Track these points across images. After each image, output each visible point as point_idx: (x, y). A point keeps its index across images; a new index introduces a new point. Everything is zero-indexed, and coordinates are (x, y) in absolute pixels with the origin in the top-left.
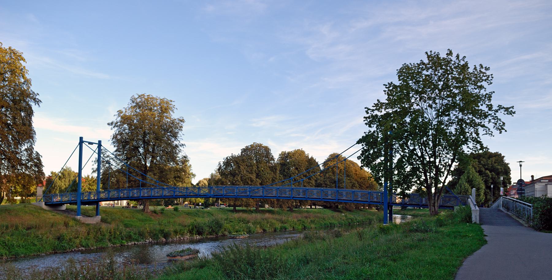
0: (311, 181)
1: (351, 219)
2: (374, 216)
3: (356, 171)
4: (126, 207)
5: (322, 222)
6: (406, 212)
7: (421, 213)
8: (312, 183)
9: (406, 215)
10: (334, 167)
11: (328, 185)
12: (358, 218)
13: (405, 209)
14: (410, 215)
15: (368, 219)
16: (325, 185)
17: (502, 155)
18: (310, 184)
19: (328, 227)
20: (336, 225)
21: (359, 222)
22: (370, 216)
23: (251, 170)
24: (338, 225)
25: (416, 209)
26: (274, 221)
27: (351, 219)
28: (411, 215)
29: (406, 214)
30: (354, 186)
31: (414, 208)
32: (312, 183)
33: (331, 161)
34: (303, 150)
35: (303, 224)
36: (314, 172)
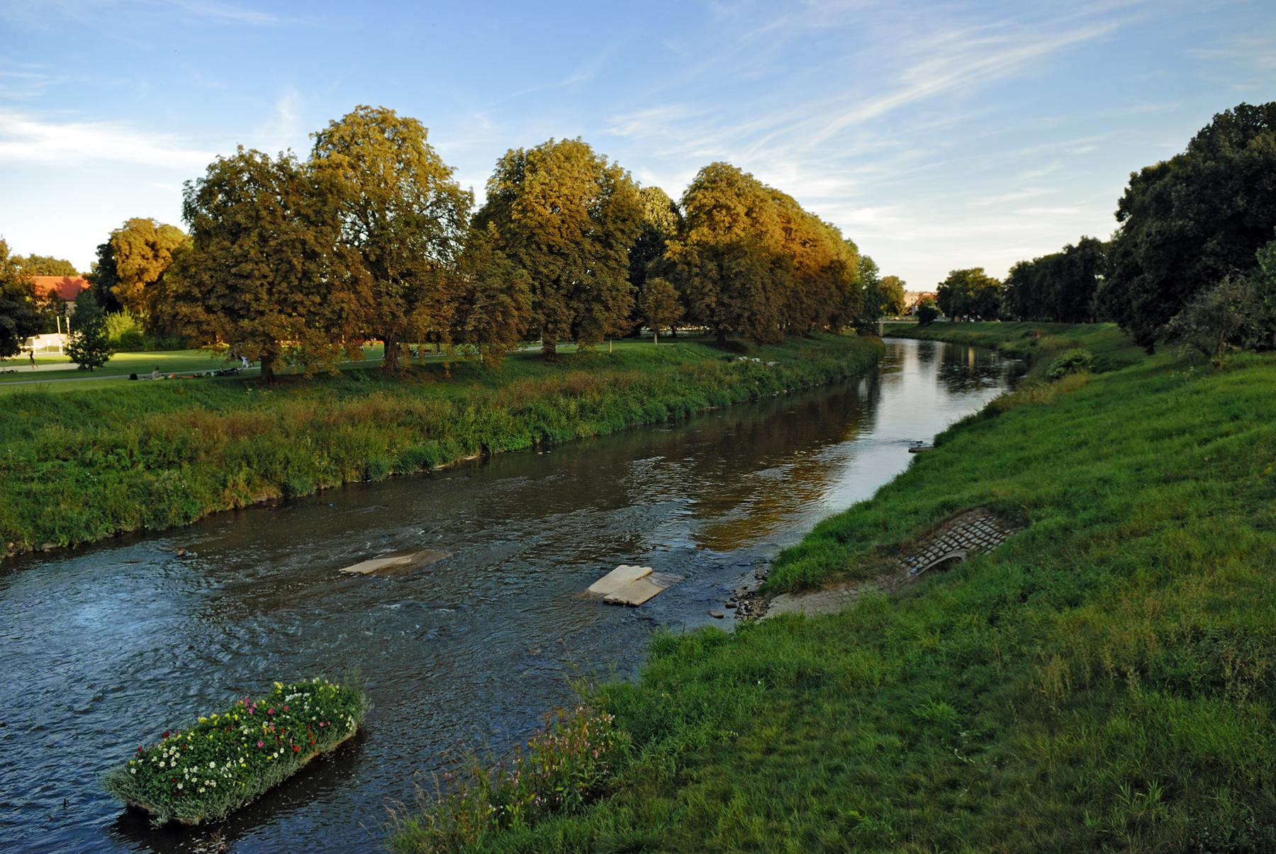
0: (612, 253)
1: (760, 380)
2: (844, 355)
3: (789, 222)
4: (386, 345)
5: (635, 407)
6: (931, 331)
7: (974, 334)
8: (616, 260)
9: (932, 339)
10: (715, 207)
11: (696, 266)
12: (788, 373)
13: (930, 324)
14: (942, 340)
15: (822, 371)
16: (686, 267)
17: (1124, 196)
18: (613, 264)
19: (659, 422)
20: (694, 409)
21: (788, 387)
22: (828, 360)
23: (317, 213)
24: (707, 407)
25: (958, 323)
26: (358, 434)
27: (760, 380)
28: (948, 341)
29: (932, 336)
30: (780, 267)
31: (953, 320)
32: (616, 260)
33: (706, 189)
34: (583, 141)
35: (542, 424)
36: (624, 221)
